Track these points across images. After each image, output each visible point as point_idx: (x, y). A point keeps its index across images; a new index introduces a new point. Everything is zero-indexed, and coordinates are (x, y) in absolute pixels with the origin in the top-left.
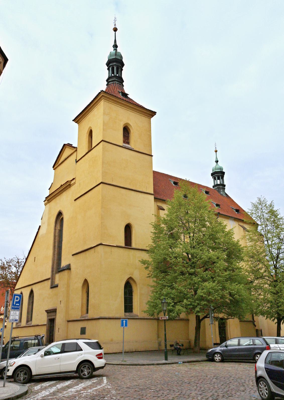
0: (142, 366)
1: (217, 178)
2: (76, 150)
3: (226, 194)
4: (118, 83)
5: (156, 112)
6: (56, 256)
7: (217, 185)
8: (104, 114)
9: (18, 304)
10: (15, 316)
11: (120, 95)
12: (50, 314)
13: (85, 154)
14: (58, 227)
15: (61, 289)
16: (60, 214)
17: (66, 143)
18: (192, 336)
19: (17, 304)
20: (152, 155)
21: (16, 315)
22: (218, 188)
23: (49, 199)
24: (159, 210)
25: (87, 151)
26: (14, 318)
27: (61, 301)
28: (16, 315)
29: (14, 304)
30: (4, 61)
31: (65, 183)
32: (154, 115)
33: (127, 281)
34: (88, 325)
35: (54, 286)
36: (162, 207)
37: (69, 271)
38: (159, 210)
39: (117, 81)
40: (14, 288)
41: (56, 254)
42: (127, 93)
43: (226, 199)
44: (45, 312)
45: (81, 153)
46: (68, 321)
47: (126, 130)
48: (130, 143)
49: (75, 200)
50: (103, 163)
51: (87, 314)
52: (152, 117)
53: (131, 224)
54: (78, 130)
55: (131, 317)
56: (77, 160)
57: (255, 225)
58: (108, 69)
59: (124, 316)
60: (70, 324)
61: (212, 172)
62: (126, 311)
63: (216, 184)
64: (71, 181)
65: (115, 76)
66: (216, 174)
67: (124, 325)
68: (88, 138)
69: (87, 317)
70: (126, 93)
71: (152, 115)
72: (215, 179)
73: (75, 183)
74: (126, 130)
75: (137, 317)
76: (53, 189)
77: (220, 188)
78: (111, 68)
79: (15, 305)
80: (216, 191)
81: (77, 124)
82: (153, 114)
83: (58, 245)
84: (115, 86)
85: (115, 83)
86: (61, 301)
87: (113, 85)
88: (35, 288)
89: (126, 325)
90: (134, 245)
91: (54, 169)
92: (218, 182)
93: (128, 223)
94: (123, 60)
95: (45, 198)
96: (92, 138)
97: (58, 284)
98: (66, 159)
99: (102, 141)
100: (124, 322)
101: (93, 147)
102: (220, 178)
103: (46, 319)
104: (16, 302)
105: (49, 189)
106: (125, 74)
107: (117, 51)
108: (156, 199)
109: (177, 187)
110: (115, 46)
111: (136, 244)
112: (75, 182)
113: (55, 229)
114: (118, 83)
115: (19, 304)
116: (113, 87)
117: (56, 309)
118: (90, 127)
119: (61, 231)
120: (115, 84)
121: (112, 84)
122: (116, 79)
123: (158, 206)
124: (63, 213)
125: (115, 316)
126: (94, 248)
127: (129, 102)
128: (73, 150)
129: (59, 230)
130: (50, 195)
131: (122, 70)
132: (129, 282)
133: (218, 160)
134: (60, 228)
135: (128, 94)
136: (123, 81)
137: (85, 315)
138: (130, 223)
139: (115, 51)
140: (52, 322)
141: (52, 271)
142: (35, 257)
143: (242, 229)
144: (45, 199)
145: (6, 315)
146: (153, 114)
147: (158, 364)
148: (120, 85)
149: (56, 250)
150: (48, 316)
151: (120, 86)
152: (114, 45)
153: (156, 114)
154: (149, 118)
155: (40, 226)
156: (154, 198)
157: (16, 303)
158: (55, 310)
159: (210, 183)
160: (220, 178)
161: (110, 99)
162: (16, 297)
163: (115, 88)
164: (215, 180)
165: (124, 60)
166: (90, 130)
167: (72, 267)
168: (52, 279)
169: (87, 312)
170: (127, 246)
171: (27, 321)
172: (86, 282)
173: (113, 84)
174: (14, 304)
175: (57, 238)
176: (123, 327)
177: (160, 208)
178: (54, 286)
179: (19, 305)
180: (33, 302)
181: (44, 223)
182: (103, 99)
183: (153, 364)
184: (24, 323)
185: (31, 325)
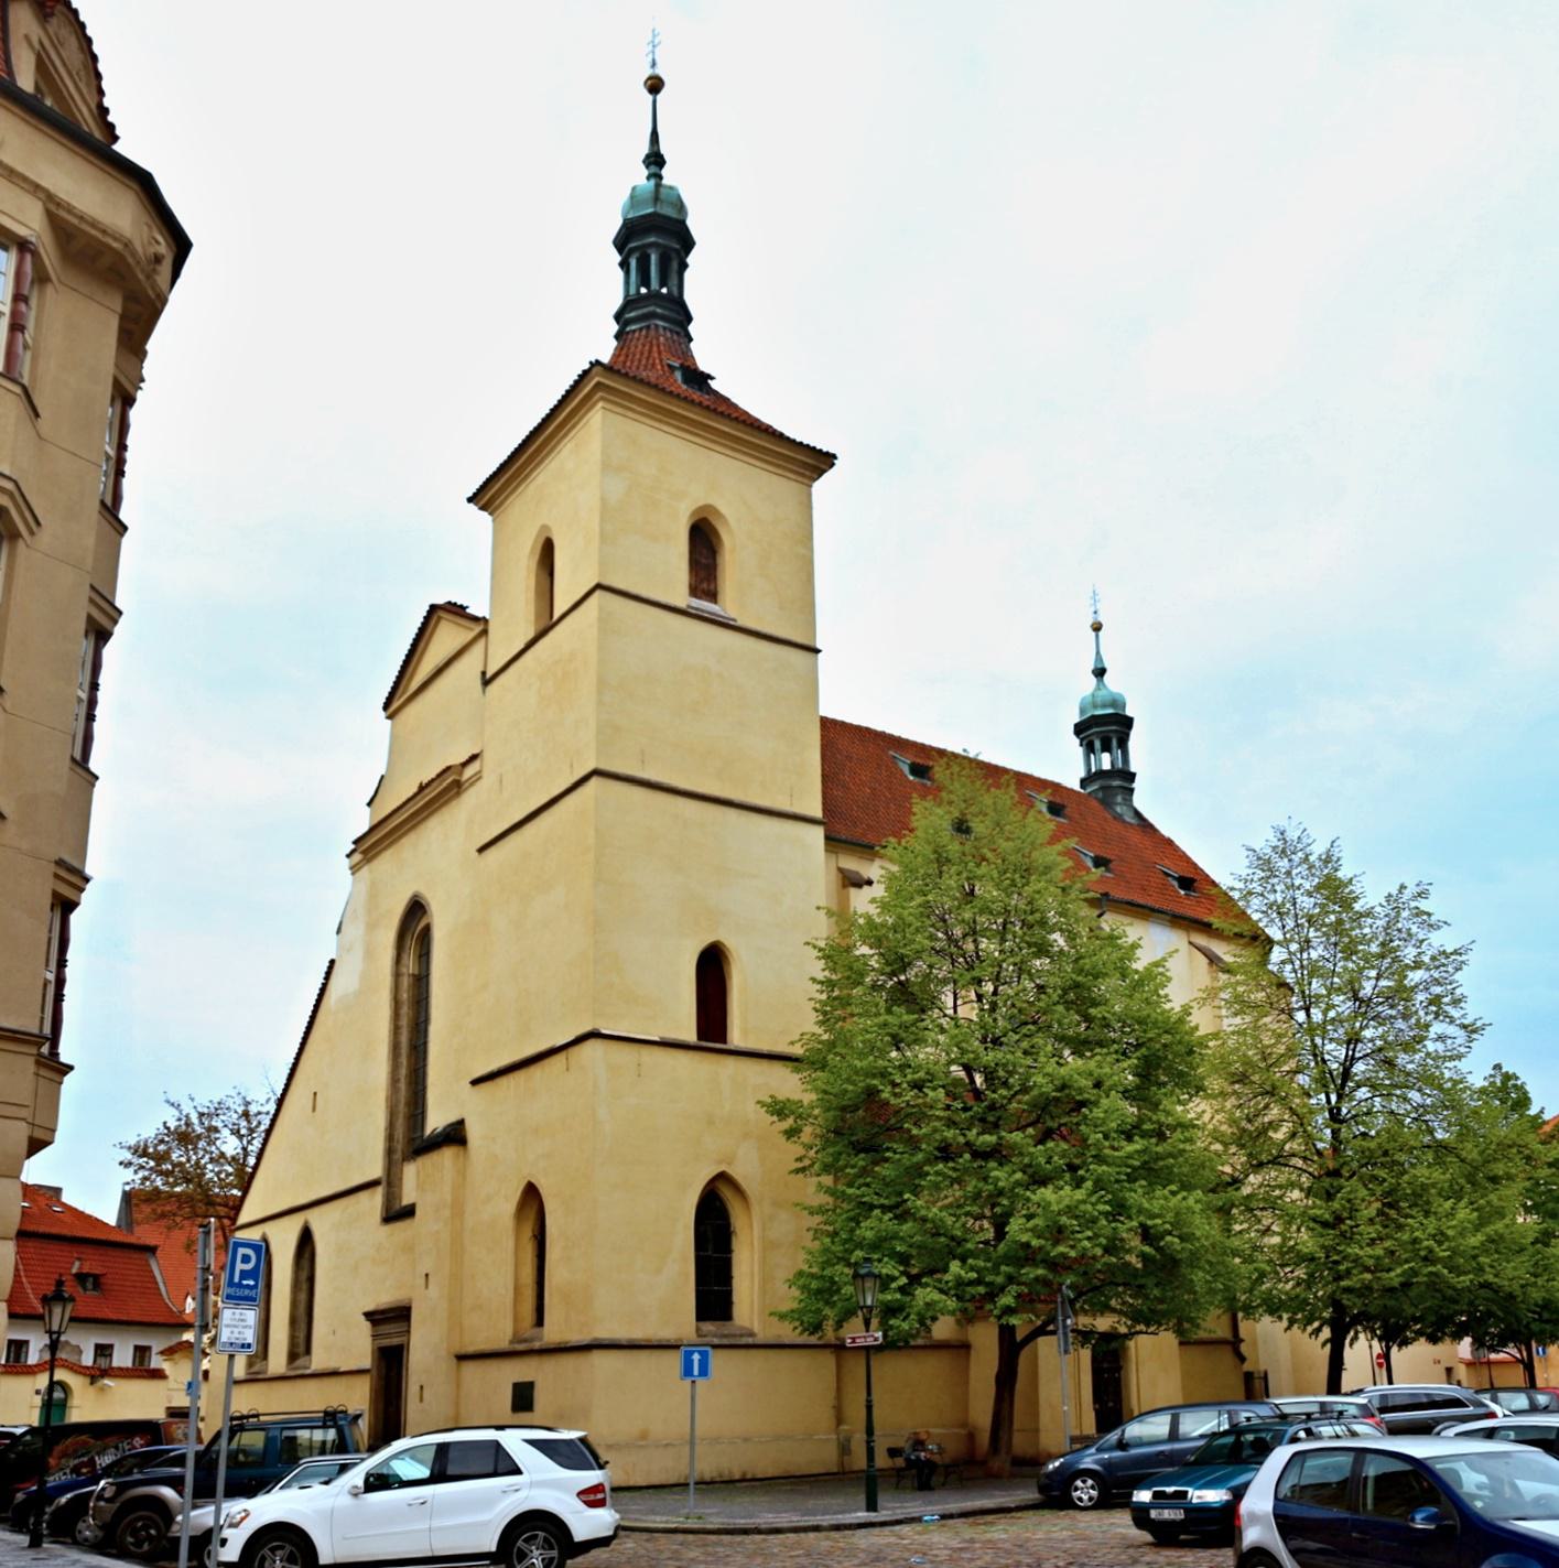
0: (771, 1537)
1: (1098, 744)
2: (485, 632)
3: (1138, 814)
4: (665, 328)
6: (403, 1085)
7: (1101, 774)
8: (607, 467)
9: (252, 1283)
12: (385, 1329)
13: (522, 646)
16: (416, 908)
17: (440, 601)
19: (245, 1282)
20: (819, 646)
22: (1102, 788)
23: (368, 847)
24: (844, 886)
25: (531, 634)
27: (427, 1275)
28: (246, 1327)
29: (236, 1280)
31: (439, 776)
32: (824, 467)
34: (545, 1375)
35: (397, 1213)
36: (857, 873)
37: (461, 1148)
38: (844, 886)
39: (662, 318)
40: (234, 1220)
43: (1135, 838)
46: (462, 1358)
47: (704, 539)
49: (481, 850)
50: (602, 684)
55: (725, 1341)
56: (488, 675)
57: (1258, 941)
58: (624, 265)
60: (470, 1369)
61: (1077, 720)
62: (702, 1315)
63: (1093, 770)
64: (465, 764)
65: (654, 297)
66: (1097, 725)
67: (696, 1372)
69: (541, 1339)
71: (818, 468)
72: (1089, 748)
73: (478, 777)
74: (704, 539)
75: (750, 1341)
78: (638, 260)
79: (240, 1285)
80: (1095, 804)
81: (485, 514)
82: (818, 462)
83: (411, 1040)
84: (654, 342)
86: (427, 1275)
87: (646, 337)
88: (319, 1220)
89: (704, 1372)
90: (737, 1037)
92: (1106, 762)
94: (689, 223)
96: (551, 574)
98: (439, 672)
99: (599, 586)
100: (692, 1359)
101: (557, 615)
104: (242, 1271)
105: (369, 804)
106: (698, 286)
107: (664, 182)
108: (833, 842)
109: (924, 785)
110: (655, 160)
111: (745, 1033)
112: (480, 772)
113: (397, 975)
115: (256, 1280)
118: (545, 528)
119: (422, 982)
120: (652, 333)
121: (641, 329)
122: (659, 310)
123: (840, 870)
127: (729, 415)
128: (472, 629)
129: (413, 975)
130: (372, 830)
131: (684, 266)
133: (1107, 665)
135: (713, 374)
136: (689, 319)
138: (722, 940)
139: (652, 182)
140: (390, 1366)
141: (389, 1152)
142: (315, 1094)
144: (353, 847)
146: (818, 462)
147: (837, 1528)
148: (678, 333)
149: (404, 1060)
150: (375, 1337)
151: (675, 337)
152: (648, 156)
153: (833, 465)
154: (806, 481)
155: (332, 962)
156: (828, 838)
159: (1066, 766)
162: (242, 1251)
163: (655, 349)
166: (541, 541)
167: (473, 1132)
168: (389, 1184)
169: (540, 1322)
171: (293, 1356)
172: (532, 1195)
173: (644, 332)
174: (236, 1280)
176: (688, 1381)
177: (849, 879)
178: (397, 1213)
179: (255, 1286)
180: (311, 1279)
182: (602, 399)
184: (277, 1362)
185: (308, 1372)
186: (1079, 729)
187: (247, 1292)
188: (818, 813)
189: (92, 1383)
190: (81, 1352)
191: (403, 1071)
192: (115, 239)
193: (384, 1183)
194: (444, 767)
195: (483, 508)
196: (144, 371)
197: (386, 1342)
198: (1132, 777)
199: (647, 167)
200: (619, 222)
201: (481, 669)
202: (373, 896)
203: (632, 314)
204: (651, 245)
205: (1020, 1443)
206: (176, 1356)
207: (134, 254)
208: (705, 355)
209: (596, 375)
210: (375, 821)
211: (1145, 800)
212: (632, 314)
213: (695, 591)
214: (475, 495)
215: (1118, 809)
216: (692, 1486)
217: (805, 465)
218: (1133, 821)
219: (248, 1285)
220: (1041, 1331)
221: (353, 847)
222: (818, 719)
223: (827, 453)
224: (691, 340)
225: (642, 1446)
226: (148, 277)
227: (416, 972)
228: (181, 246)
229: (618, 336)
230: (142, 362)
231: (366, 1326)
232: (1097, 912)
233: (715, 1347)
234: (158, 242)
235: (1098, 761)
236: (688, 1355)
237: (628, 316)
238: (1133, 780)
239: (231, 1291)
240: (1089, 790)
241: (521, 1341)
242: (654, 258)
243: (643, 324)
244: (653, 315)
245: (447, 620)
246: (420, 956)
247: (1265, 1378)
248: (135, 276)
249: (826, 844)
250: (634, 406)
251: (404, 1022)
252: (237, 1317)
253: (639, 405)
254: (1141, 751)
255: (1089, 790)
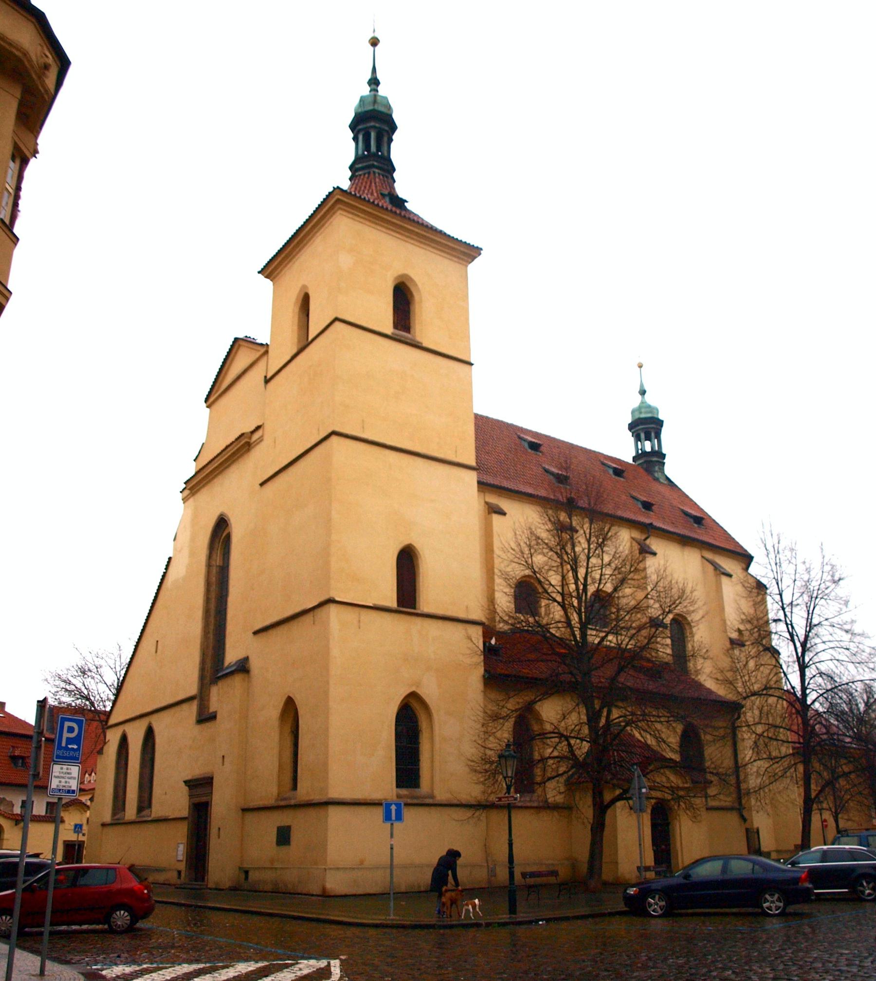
2: (266, 352)
5: (481, 249)
6: (211, 636)
7: (645, 453)
9: (75, 747)
10: (68, 780)
11: (386, 203)
12: (199, 791)
14: (218, 560)
15: (224, 725)
16: (222, 525)
17: (241, 336)
18: (583, 853)
19: (70, 746)
20: (472, 362)
21: (69, 776)
22: (646, 462)
24: (489, 513)
25: (295, 351)
26: (64, 786)
27: (223, 757)
29: (64, 744)
30: (59, 65)
31: (237, 439)
32: (474, 254)
33: (404, 702)
34: (298, 821)
36: (497, 506)
37: (246, 675)
38: (489, 513)
39: (377, 168)
41: (211, 631)
42: (404, 198)
44: (183, 784)
45: (275, 361)
46: (245, 810)
48: (412, 330)
51: (294, 792)
52: (470, 260)
53: (414, 547)
54: (273, 305)
55: (415, 801)
56: (268, 377)
58: (355, 139)
59: (395, 798)
60: (250, 817)
62: (400, 784)
64: (253, 432)
65: (371, 156)
66: (642, 424)
67: (393, 817)
68: (299, 318)
69: (296, 798)
70: (401, 199)
72: (638, 438)
73: (261, 439)
76: (204, 461)
77: (652, 461)
79: (66, 748)
80: (642, 470)
81: (268, 281)
83: (216, 608)
84: (373, 180)
85: (372, 172)
86: (223, 757)
89: (399, 817)
91: (207, 407)
93: (406, 543)
94: (394, 116)
95: (185, 483)
96: (308, 315)
97: (216, 712)
101: (310, 339)
102: (653, 435)
103: (188, 804)
104: (68, 738)
105: (195, 460)
108: (483, 486)
110: (374, 82)
112: (262, 436)
113: (209, 566)
114: (379, 174)
116: (366, 183)
117: (212, 778)
122: (375, 163)
123: (487, 503)
124: (229, 520)
125: (370, 798)
126: (312, 613)
129: (219, 566)
130: (197, 473)
131: (390, 140)
132: (410, 706)
133: (646, 389)
134: (223, 563)
136: (394, 170)
137: (290, 794)
138: (413, 543)
139: (373, 93)
141: (202, 678)
143: (710, 568)
144: (184, 486)
145: (35, 771)
148: (387, 177)
149: (212, 619)
150: (191, 796)
152: (370, 80)
153: (480, 254)
154: (464, 263)
155: (170, 559)
156: (480, 483)
157: (67, 744)
158: (210, 781)
160: (653, 435)
161: (356, 208)
162: (67, 724)
163: (373, 184)
164: (639, 443)
165: (396, 117)
166: (302, 294)
167: (255, 665)
169: (295, 787)
170: (403, 607)
171: (140, 809)
173: (367, 176)
174: (64, 744)
175: (213, 588)
176: (388, 824)
177: (492, 508)
178: (206, 717)
179: (78, 749)
181: (180, 551)
183: (567, 919)
184: (131, 812)
185: (150, 819)
186: (631, 427)
187: (72, 753)
188: (472, 462)
189: (16, 825)
190: (13, 805)
191: (212, 627)
192: (18, 50)
193: (198, 698)
194: (239, 434)
195: (267, 277)
196: (39, 141)
197: (197, 800)
198: (663, 456)
199: (370, 86)
200: (353, 115)
201: (265, 374)
202: (195, 518)
203: (360, 165)
204: (374, 127)
205: (607, 875)
206: (70, 808)
207: (30, 61)
208: (401, 189)
209: (337, 194)
210: (198, 469)
211: (672, 469)
212: (360, 165)
213: (396, 326)
214: (262, 269)
215: (656, 475)
216: (392, 895)
217: (464, 254)
218: (665, 482)
219: (73, 749)
220: (619, 798)
221: (184, 486)
222: (473, 416)
223: (477, 247)
224: (394, 181)
225: (361, 868)
226: (39, 78)
227: (221, 564)
228: (64, 63)
229: (351, 179)
230: (36, 137)
231: (185, 789)
232: (643, 537)
233: (406, 805)
234: (47, 56)
235: (643, 446)
236: (388, 806)
237: (357, 166)
238: (664, 458)
239: (60, 753)
240: (637, 463)
241: (282, 800)
242: (373, 135)
243: (366, 171)
244: (373, 166)
245: (245, 346)
246: (224, 555)
247: (758, 832)
248: (30, 76)
249: (478, 487)
250: (360, 214)
251: (213, 595)
252: (65, 771)
253: (362, 213)
254: (669, 441)
255: (637, 463)
